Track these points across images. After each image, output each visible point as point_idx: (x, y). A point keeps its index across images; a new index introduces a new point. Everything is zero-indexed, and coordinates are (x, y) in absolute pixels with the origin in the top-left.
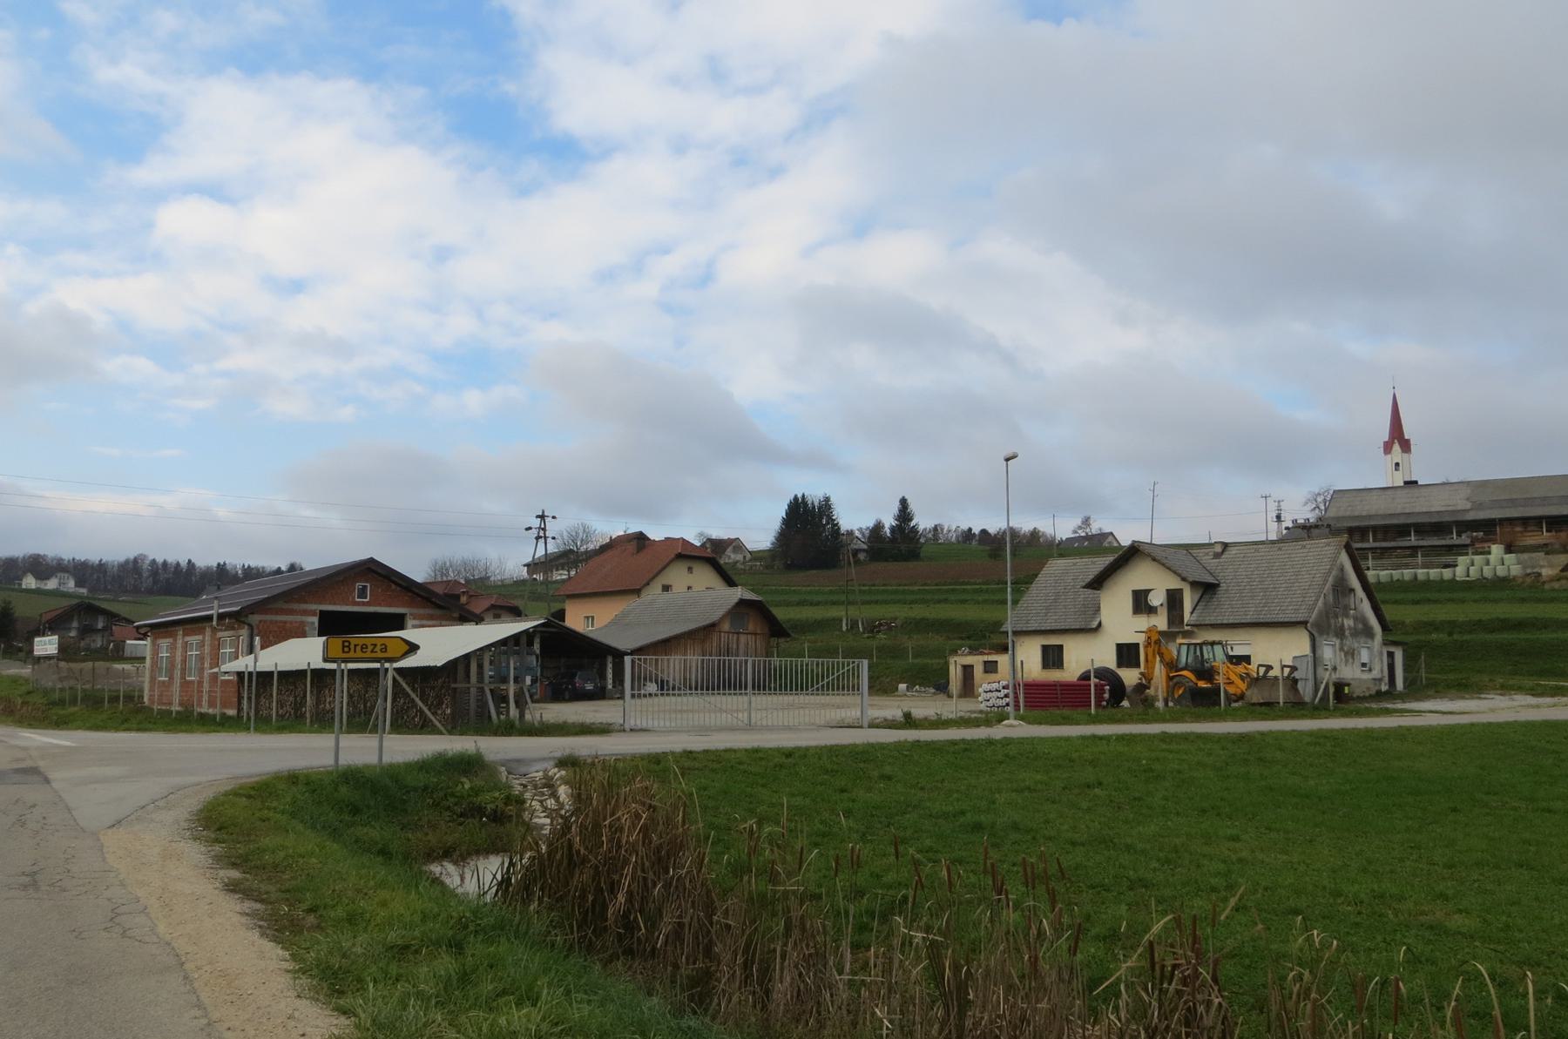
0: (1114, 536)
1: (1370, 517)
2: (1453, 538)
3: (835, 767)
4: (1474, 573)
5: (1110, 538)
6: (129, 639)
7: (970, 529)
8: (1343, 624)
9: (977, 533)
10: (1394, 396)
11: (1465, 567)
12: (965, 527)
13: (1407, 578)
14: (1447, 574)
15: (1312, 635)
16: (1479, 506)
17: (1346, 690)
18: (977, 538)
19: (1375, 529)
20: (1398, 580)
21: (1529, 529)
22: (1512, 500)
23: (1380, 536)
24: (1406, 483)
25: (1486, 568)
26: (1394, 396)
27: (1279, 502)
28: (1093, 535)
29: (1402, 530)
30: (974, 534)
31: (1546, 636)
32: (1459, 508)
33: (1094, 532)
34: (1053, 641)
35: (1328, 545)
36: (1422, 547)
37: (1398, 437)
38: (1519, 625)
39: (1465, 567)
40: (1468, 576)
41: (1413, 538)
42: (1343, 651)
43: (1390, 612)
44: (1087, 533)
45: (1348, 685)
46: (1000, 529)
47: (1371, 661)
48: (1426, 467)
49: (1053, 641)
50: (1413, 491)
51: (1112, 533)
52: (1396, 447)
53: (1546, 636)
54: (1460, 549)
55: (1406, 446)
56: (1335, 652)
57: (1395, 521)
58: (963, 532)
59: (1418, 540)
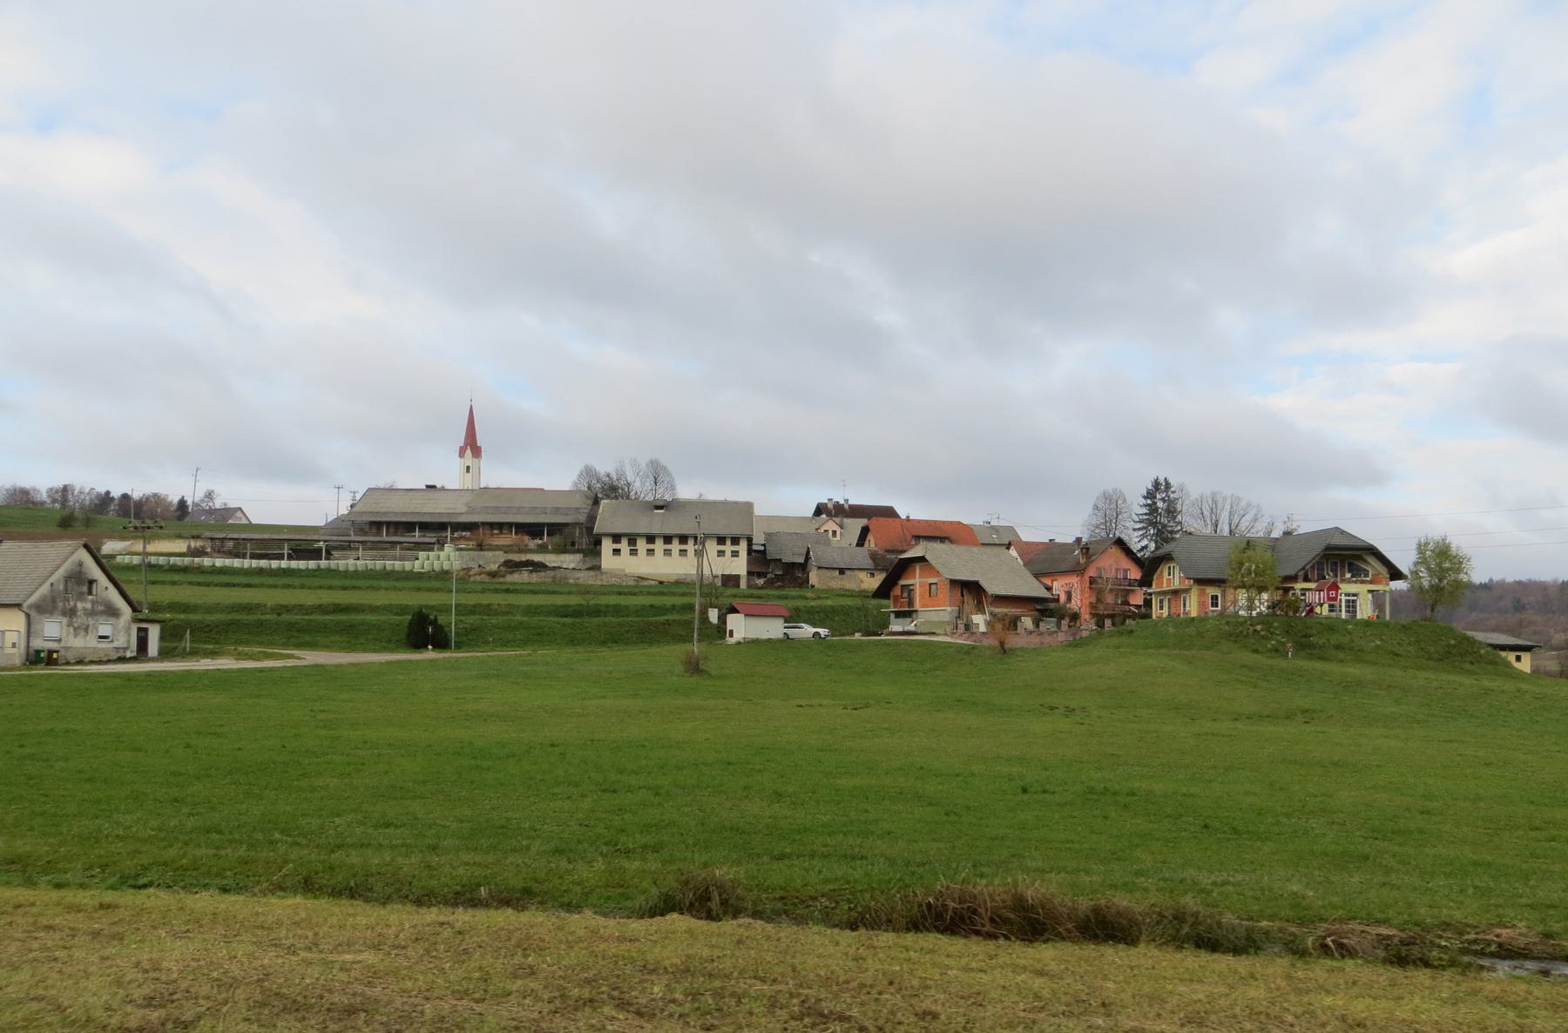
0: (243, 512)
1: (385, 514)
2: (415, 536)
3: (717, 953)
4: (427, 567)
5: (239, 514)
6: (111, 537)
7: (108, 493)
8: (75, 606)
9: (116, 497)
10: (471, 407)
11: (425, 561)
12: (102, 490)
13: (378, 568)
14: (408, 565)
15: (28, 616)
16: (471, 510)
17: (55, 656)
18: (116, 502)
19: (388, 524)
20: (371, 569)
21: (504, 531)
22: (497, 508)
23: (392, 530)
24: (428, 487)
25: (436, 562)
26: (471, 407)
27: (354, 493)
28: (216, 510)
29: (409, 527)
30: (113, 498)
31: (360, 617)
32: (457, 511)
33: (217, 506)
34: (144, 625)
35: (69, 545)
36: (401, 543)
37: (471, 445)
38: (338, 609)
39: (425, 561)
40: (423, 568)
41: (417, 534)
42: (73, 626)
43: (135, 596)
44: (210, 507)
45: (57, 652)
46: (144, 495)
47: (113, 635)
48: (498, 474)
49: (144, 625)
50: (431, 494)
51: (240, 509)
52: (469, 452)
53: (360, 617)
54: (419, 546)
55: (477, 452)
56: (61, 628)
57: (404, 519)
58: (99, 495)
59: (422, 536)
